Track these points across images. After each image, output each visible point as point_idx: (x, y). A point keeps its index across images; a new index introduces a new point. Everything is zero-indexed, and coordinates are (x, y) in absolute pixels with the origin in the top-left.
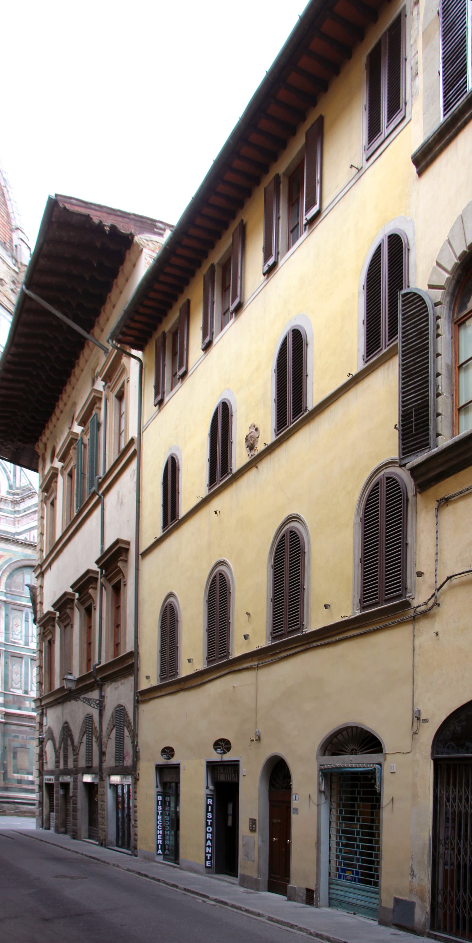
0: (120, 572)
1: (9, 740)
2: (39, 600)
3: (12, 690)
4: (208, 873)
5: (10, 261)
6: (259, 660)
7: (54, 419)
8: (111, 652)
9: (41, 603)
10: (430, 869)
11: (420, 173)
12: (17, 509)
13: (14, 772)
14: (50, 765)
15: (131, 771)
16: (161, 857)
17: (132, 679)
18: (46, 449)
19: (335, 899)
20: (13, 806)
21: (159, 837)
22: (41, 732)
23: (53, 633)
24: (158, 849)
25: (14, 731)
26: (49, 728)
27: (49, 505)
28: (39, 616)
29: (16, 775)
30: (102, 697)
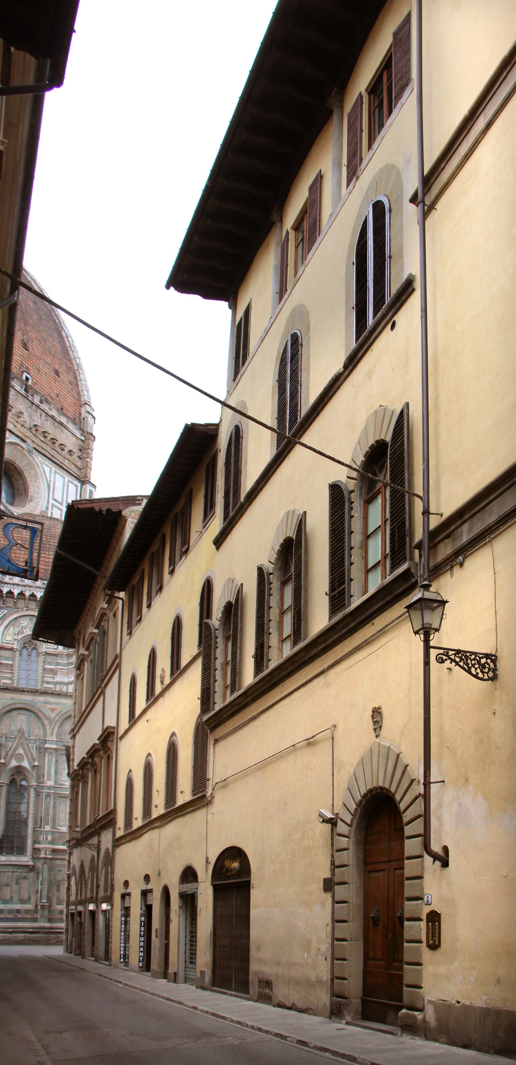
0: (109, 749)
1: (55, 874)
2: (71, 758)
3: (58, 828)
4: (140, 971)
5: (78, 434)
6: (161, 822)
7: (84, 615)
8: (105, 808)
9: (73, 760)
10: (212, 950)
11: (218, 548)
12: (70, 661)
13: (57, 904)
14: (73, 898)
15: (109, 900)
16: (123, 964)
17: (111, 830)
18: (80, 635)
19: (189, 978)
20: (55, 935)
21: (122, 949)
22: (69, 868)
23: (78, 787)
24: (121, 958)
25: (59, 865)
26: (74, 865)
27: (80, 680)
28: (71, 771)
29: (58, 906)
30: (99, 842)
